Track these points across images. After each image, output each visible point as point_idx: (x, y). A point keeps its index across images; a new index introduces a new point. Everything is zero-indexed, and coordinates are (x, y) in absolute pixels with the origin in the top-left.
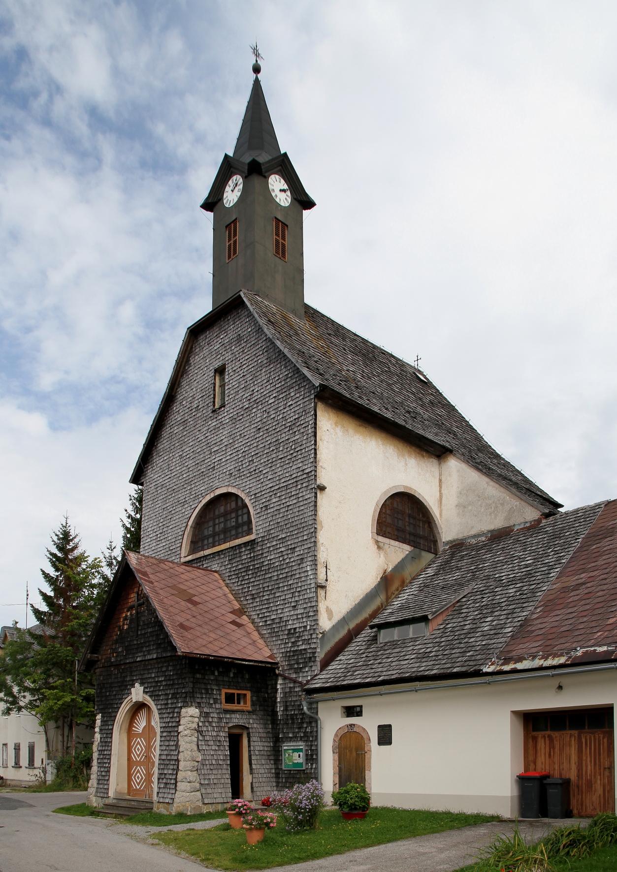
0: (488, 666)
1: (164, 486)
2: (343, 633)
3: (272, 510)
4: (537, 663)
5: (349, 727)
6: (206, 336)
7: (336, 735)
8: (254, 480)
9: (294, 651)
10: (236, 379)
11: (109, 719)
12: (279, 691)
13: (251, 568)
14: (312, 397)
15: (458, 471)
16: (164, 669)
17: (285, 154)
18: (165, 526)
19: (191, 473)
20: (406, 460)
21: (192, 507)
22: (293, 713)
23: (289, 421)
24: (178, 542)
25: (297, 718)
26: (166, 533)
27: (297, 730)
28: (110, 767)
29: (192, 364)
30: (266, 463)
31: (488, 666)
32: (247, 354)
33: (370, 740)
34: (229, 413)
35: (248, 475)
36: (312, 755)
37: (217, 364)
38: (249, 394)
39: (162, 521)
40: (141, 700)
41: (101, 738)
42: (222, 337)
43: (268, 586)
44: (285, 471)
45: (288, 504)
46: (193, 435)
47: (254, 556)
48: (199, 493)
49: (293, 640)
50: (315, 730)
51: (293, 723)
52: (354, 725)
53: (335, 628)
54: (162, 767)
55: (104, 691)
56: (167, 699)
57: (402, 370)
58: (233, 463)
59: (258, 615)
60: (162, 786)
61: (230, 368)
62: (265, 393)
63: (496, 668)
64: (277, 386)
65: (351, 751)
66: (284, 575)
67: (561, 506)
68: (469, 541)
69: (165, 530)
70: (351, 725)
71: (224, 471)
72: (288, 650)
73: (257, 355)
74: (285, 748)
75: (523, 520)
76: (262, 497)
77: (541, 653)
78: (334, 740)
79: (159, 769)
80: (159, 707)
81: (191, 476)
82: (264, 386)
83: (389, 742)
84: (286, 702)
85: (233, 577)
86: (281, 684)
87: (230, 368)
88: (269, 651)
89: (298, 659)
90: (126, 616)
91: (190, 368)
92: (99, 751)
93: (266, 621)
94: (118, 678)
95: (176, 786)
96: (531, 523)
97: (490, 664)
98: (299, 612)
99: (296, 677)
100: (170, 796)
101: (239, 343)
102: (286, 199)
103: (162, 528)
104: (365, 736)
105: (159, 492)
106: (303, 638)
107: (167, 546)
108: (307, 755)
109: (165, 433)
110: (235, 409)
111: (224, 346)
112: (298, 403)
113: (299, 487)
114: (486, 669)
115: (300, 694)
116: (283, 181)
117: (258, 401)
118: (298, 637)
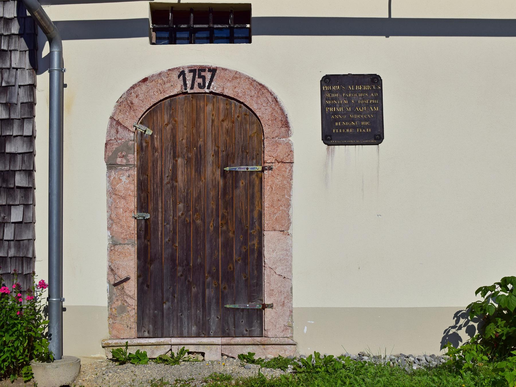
5: (189, 77)
17: (249, 40)
33: (286, 124)
52: (213, 71)
67: (41, 362)
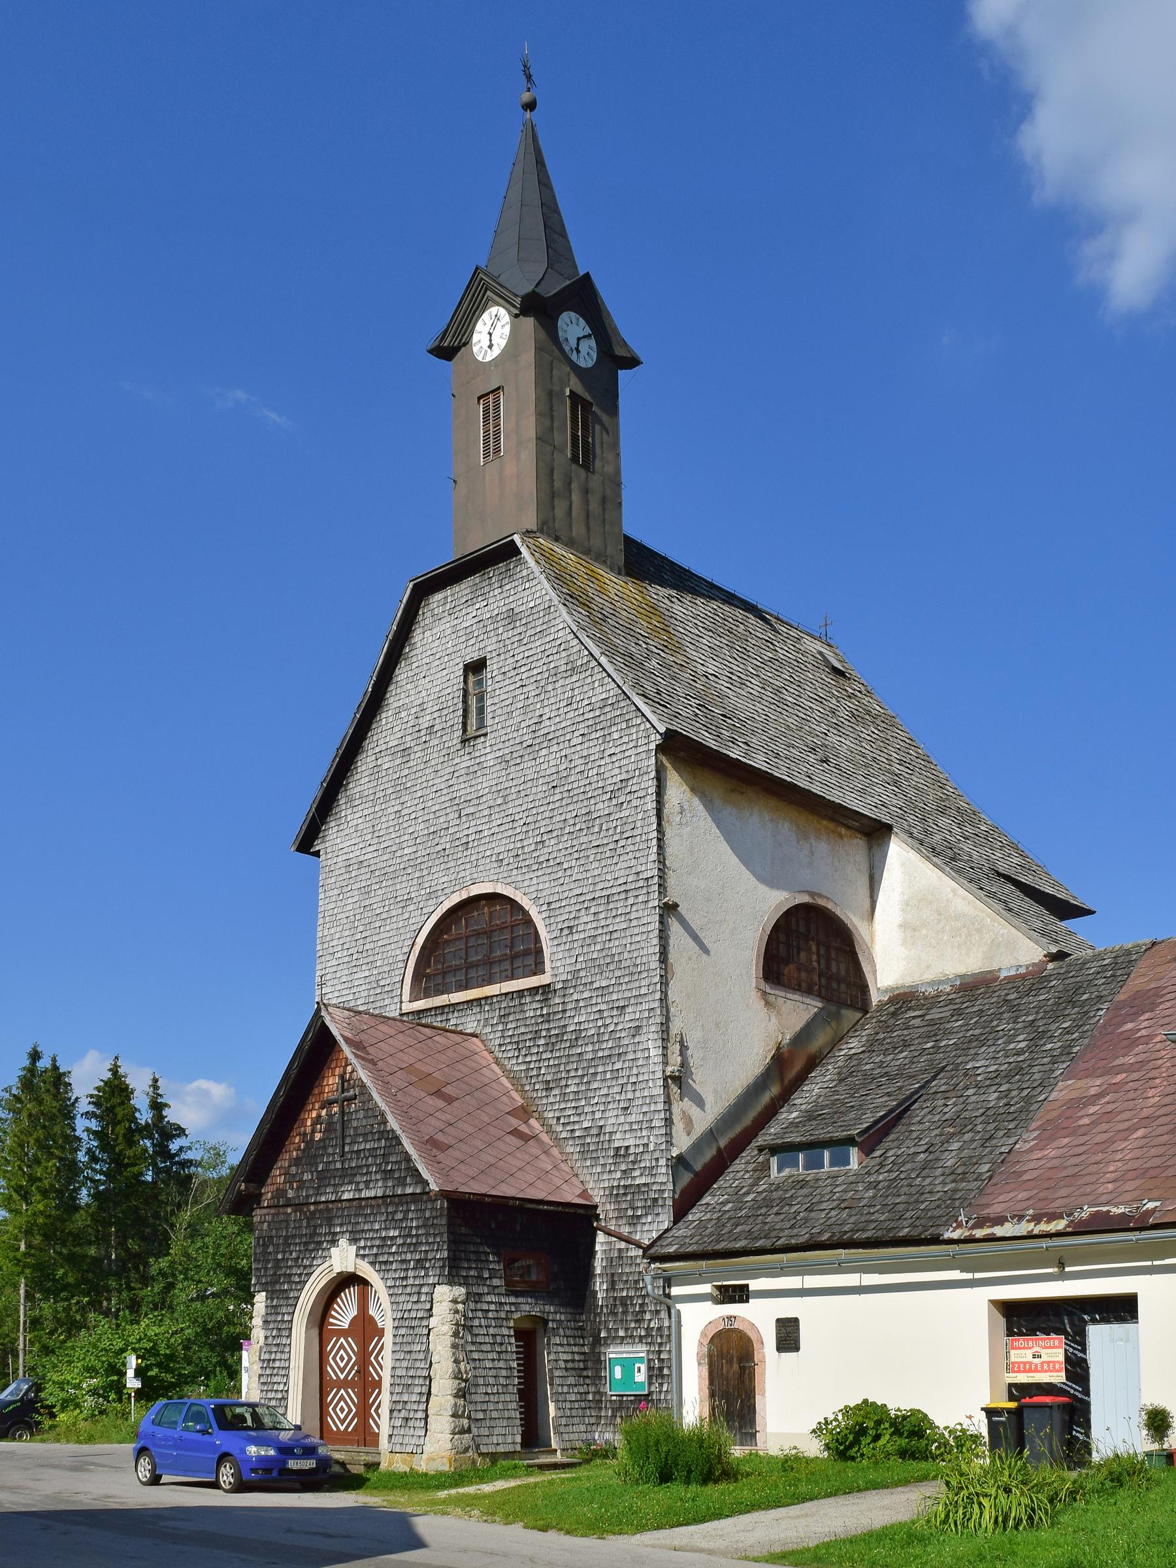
0: (951, 1229)
1: (365, 864)
2: (709, 1154)
3: (582, 936)
4: (1024, 1228)
6: (446, 598)
7: (703, 1334)
8: (546, 878)
9: (625, 1187)
10: (507, 689)
11: (282, 1299)
12: (599, 1256)
13: (544, 1033)
14: (653, 746)
15: (903, 865)
16: (399, 1216)
17: (587, 276)
18: (368, 940)
19: (420, 847)
20: (811, 844)
21: (425, 910)
22: (624, 1294)
23: (609, 782)
24: (397, 972)
25: (632, 1304)
26: (370, 953)
27: (633, 1325)
28: (287, 1391)
29: (419, 645)
30: (570, 851)
31: (951, 1229)
32: (529, 646)
33: (762, 1343)
34: (495, 748)
35: (535, 867)
36: (661, 1369)
37: (472, 655)
38: (533, 721)
39: (361, 928)
40: (351, 1269)
41: (266, 1338)
42: (477, 606)
43: (577, 1069)
44: (605, 870)
45: (611, 928)
46: (424, 779)
47: (549, 1014)
48: (439, 887)
49: (623, 1167)
50: (666, 1324)
51: (625, 1312)
52: (735, 1317)
53: (697, 1147)
54: (398, 1389)
55: (271, 1249)
56: (406, 1270)
57: (798, 651)
58: (504, 841)
59: (558, 1119)
60: (398, 1423)
61: (495, 667)
62: (563, 724)
63: (963, 1233)
64: (586, 716)
65: (730, 1362)
66: (606, 1053)
68: (923, 990)
69: (367, 947)
70: (729, 1318)
71: (488, 853)
72: (615, 1184)
73: (547, 653)
74: (611, 1356)
75: (1014, 963)
76: (562, 911)
77: (1031, 1212)
78: (701, 1343)
79: (392, 1393)
80: (389, 1283)
81: (419, 854)
82: (561, 711)
83: (796, 1348)
84: (613, 1275)
85: (509, 1047)
86: (602, 1243)
87: (495, 667)
88: (580, 1185)
89: (633, 1200)
90: (319, 1116)
91: (414, 652)
92: (263, 1361)
93: (573, 1131)
94: (300, 1227)
95: (426, 1423)
96: (1027, 968)
97: (954, 1225)
98: (633, 1118)
99: (630, 1233)
100: (414, 1441)
101: (512, 626)
102: (588, 354)
103: (361, 942)
104: (753, 1337)
105: (353, 874)
106: (643, 1165)
107: (373, 978)
108: (650, 1369)
109: (365, 763)
110: (507, 744)
111: (481, 624)
112: (627, 754)
113: (631, 901)
114: (949, 1235)
115: (638, 1261)
116: (582, 322)
117: (550, 737)
118: (634, 1162)
